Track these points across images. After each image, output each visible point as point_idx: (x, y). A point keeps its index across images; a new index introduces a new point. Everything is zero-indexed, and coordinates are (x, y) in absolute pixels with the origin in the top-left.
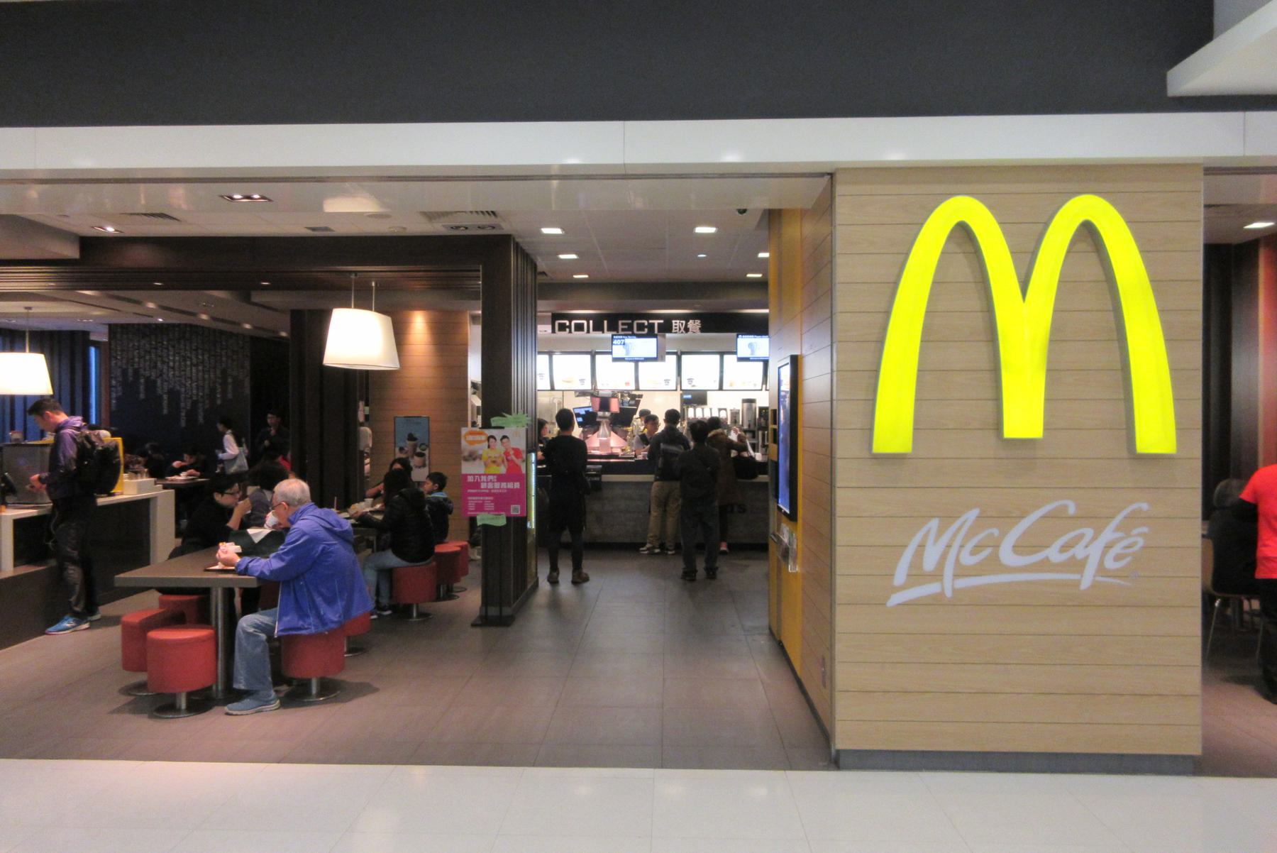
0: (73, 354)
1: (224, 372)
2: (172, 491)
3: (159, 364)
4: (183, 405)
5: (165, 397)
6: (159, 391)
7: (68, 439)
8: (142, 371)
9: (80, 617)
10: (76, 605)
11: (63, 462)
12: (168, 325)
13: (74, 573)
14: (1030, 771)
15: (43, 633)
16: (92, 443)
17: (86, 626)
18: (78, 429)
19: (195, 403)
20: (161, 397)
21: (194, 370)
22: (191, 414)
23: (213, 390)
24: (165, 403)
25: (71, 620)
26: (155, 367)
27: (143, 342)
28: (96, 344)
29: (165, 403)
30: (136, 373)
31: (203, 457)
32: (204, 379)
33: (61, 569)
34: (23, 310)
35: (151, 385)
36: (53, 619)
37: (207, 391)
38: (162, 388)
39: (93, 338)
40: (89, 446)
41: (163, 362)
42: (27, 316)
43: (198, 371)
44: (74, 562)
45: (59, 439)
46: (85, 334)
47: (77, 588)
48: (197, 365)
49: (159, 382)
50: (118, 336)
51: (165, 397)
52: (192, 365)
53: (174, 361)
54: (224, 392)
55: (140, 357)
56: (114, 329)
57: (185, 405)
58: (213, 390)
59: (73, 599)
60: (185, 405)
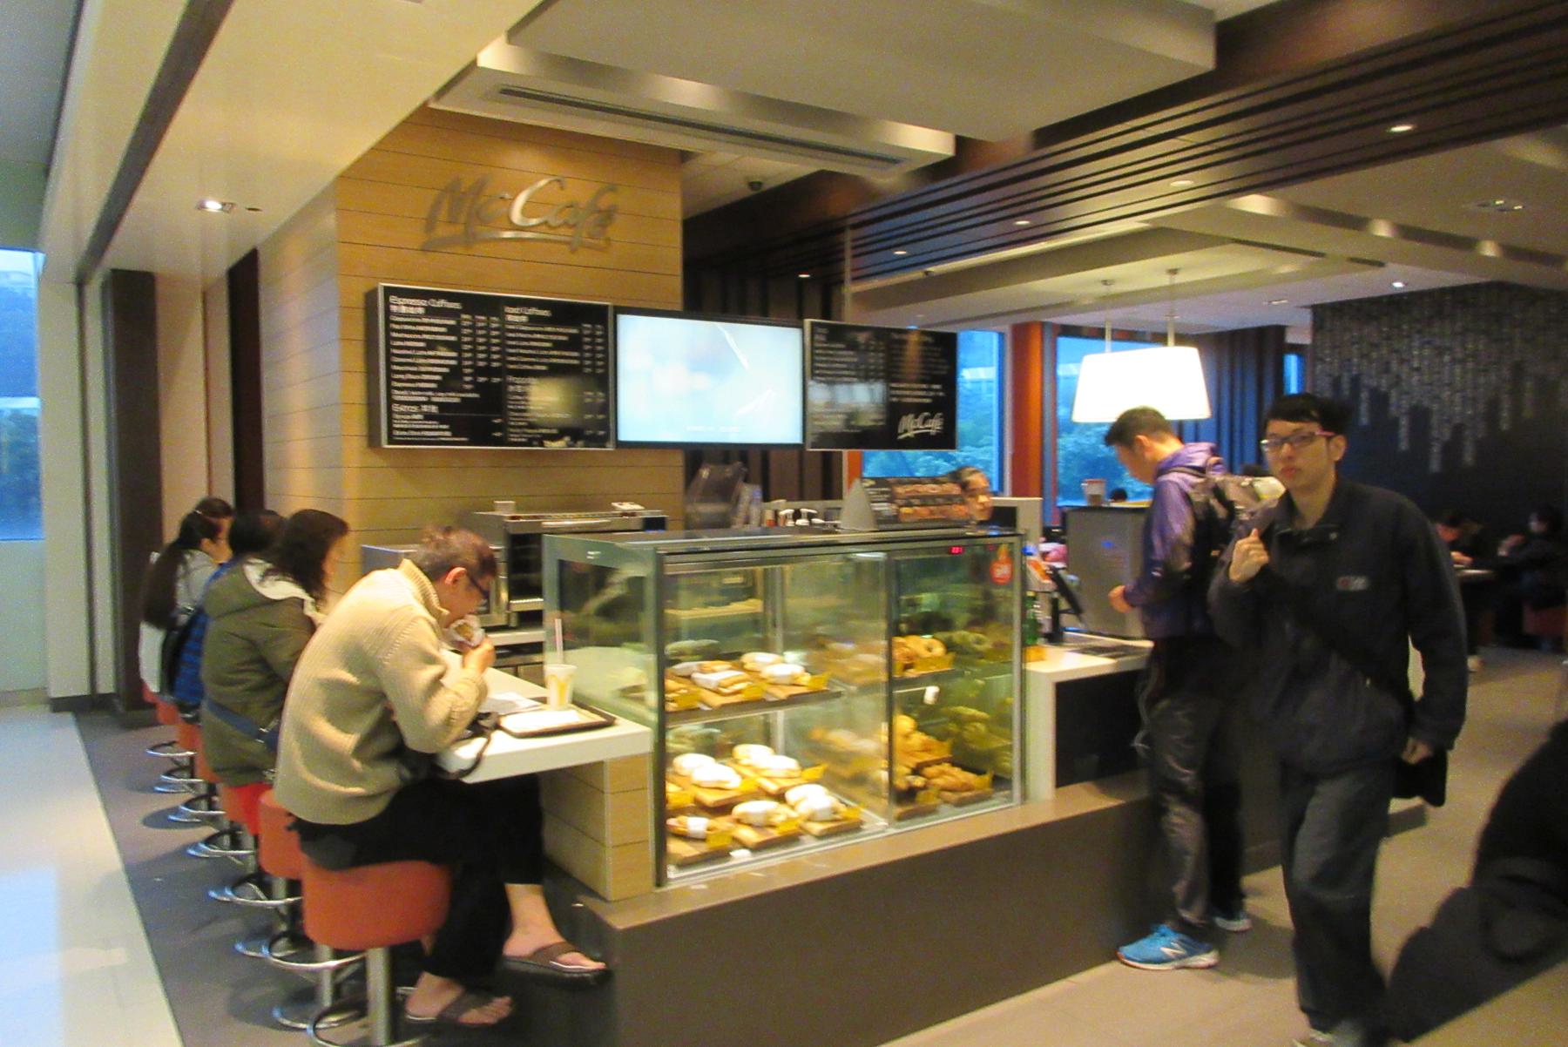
0: (1260, 366)
1: (1518, 370)
2: (388, 776)
3: (1394, 366)
4: (1435, 433)
5: (1404, 422)
6: (1393, 411)
7: (1174, 495)
8: (1366, 381)
9: (1198, 936)
10: (1187, 905)
11: (1159, 553)
12: (1411, 294)
13: (1184, 825)
14: (120, 176)
15: (1113, 956)
16: (1229, 505)
17: (1207, 959)
18: (1200, 471)
19: (1458, 430)
20: (1396, 422)
21: (1458, 370)
22: (1452, 449)
23: (1494, 405)
24: (1403, 432)
25: (1173, 938)
26: (1387, 370)
27: (1366, 331)
28: (1297, 349)
29: (1403, 432)
30: (1356, 382)
31: (1475, 528)
32: (1476, 387)
33: (1153, 812)
34: (1166, 280)
35: (1380, 401)
36: (1140, 930)
37: (1481, 407)
38: (1399, 406)
39: (1291, 338)
40: (1221, 512)
41: (1402, 362)
42: (1170, 294)
43: (1465, 372)
44: (1186, 798)
45: (1158, 494)
46: (1280, 330)
47: (1189, 861)
48: (1463, 361)
49: (1394, 394)
50: (1328, 325)
51: (1404, 422)
52: (1454, 361)
53: (1421, 358)
54: (1516, 410)
55: (1362, 356)
56: (1323, 315)
57: (1440, 433)
58: (1494, 405)
59: (1180, 888)
60: (1440, 433)
